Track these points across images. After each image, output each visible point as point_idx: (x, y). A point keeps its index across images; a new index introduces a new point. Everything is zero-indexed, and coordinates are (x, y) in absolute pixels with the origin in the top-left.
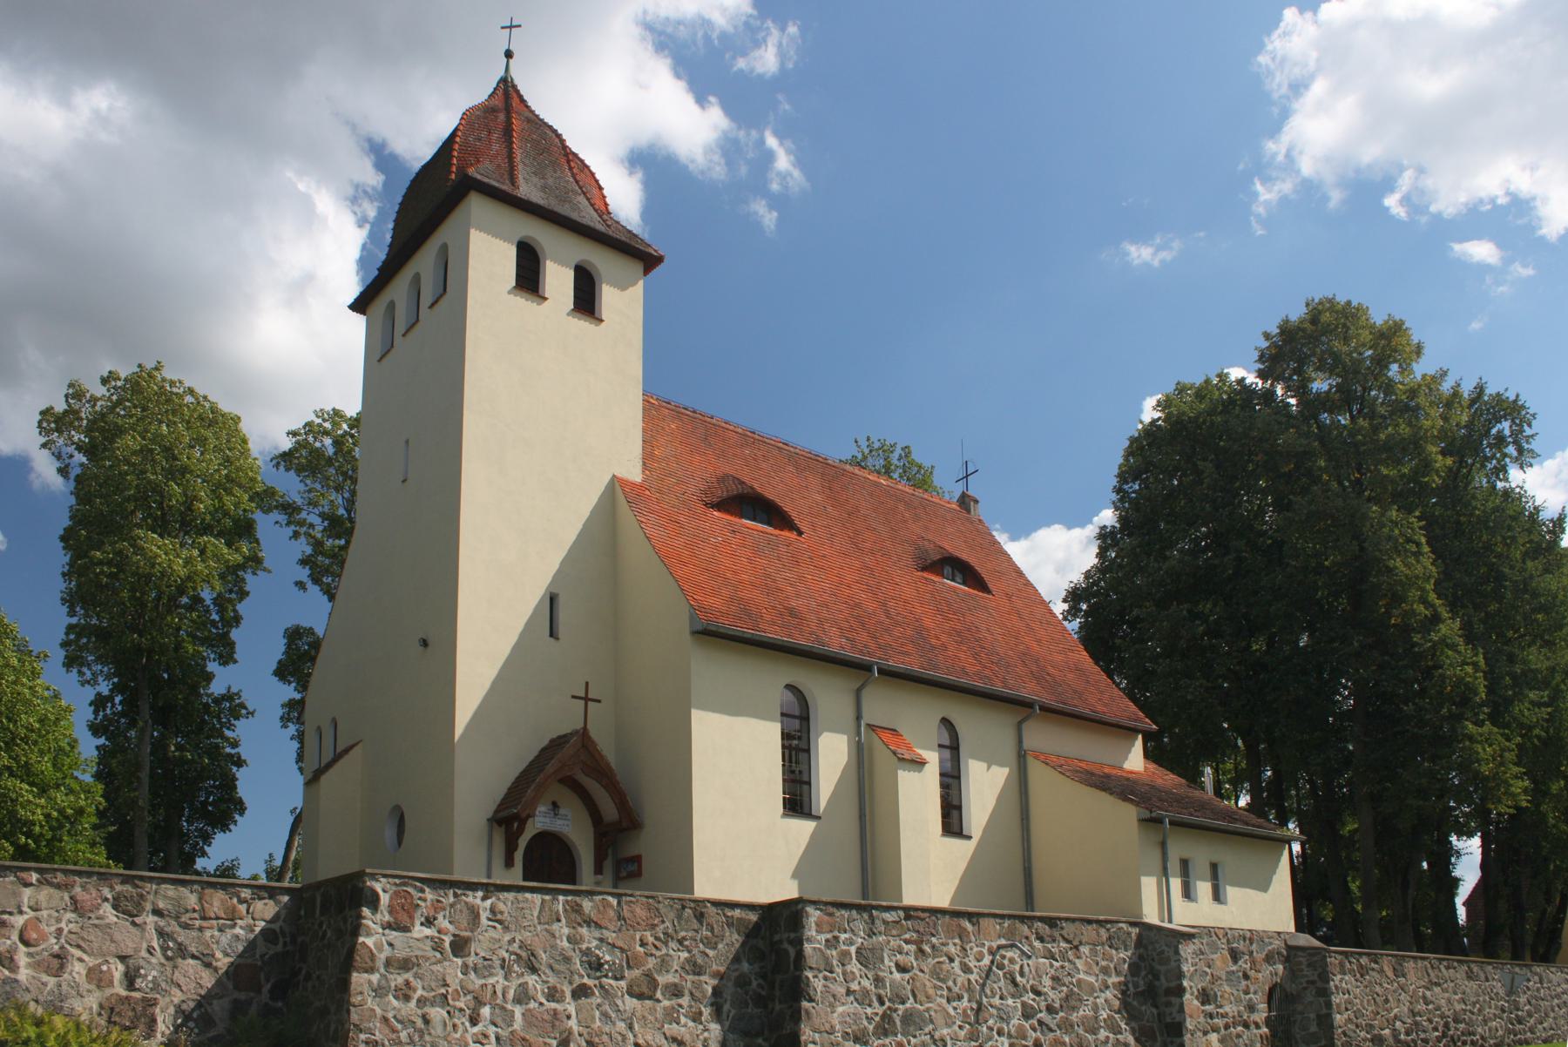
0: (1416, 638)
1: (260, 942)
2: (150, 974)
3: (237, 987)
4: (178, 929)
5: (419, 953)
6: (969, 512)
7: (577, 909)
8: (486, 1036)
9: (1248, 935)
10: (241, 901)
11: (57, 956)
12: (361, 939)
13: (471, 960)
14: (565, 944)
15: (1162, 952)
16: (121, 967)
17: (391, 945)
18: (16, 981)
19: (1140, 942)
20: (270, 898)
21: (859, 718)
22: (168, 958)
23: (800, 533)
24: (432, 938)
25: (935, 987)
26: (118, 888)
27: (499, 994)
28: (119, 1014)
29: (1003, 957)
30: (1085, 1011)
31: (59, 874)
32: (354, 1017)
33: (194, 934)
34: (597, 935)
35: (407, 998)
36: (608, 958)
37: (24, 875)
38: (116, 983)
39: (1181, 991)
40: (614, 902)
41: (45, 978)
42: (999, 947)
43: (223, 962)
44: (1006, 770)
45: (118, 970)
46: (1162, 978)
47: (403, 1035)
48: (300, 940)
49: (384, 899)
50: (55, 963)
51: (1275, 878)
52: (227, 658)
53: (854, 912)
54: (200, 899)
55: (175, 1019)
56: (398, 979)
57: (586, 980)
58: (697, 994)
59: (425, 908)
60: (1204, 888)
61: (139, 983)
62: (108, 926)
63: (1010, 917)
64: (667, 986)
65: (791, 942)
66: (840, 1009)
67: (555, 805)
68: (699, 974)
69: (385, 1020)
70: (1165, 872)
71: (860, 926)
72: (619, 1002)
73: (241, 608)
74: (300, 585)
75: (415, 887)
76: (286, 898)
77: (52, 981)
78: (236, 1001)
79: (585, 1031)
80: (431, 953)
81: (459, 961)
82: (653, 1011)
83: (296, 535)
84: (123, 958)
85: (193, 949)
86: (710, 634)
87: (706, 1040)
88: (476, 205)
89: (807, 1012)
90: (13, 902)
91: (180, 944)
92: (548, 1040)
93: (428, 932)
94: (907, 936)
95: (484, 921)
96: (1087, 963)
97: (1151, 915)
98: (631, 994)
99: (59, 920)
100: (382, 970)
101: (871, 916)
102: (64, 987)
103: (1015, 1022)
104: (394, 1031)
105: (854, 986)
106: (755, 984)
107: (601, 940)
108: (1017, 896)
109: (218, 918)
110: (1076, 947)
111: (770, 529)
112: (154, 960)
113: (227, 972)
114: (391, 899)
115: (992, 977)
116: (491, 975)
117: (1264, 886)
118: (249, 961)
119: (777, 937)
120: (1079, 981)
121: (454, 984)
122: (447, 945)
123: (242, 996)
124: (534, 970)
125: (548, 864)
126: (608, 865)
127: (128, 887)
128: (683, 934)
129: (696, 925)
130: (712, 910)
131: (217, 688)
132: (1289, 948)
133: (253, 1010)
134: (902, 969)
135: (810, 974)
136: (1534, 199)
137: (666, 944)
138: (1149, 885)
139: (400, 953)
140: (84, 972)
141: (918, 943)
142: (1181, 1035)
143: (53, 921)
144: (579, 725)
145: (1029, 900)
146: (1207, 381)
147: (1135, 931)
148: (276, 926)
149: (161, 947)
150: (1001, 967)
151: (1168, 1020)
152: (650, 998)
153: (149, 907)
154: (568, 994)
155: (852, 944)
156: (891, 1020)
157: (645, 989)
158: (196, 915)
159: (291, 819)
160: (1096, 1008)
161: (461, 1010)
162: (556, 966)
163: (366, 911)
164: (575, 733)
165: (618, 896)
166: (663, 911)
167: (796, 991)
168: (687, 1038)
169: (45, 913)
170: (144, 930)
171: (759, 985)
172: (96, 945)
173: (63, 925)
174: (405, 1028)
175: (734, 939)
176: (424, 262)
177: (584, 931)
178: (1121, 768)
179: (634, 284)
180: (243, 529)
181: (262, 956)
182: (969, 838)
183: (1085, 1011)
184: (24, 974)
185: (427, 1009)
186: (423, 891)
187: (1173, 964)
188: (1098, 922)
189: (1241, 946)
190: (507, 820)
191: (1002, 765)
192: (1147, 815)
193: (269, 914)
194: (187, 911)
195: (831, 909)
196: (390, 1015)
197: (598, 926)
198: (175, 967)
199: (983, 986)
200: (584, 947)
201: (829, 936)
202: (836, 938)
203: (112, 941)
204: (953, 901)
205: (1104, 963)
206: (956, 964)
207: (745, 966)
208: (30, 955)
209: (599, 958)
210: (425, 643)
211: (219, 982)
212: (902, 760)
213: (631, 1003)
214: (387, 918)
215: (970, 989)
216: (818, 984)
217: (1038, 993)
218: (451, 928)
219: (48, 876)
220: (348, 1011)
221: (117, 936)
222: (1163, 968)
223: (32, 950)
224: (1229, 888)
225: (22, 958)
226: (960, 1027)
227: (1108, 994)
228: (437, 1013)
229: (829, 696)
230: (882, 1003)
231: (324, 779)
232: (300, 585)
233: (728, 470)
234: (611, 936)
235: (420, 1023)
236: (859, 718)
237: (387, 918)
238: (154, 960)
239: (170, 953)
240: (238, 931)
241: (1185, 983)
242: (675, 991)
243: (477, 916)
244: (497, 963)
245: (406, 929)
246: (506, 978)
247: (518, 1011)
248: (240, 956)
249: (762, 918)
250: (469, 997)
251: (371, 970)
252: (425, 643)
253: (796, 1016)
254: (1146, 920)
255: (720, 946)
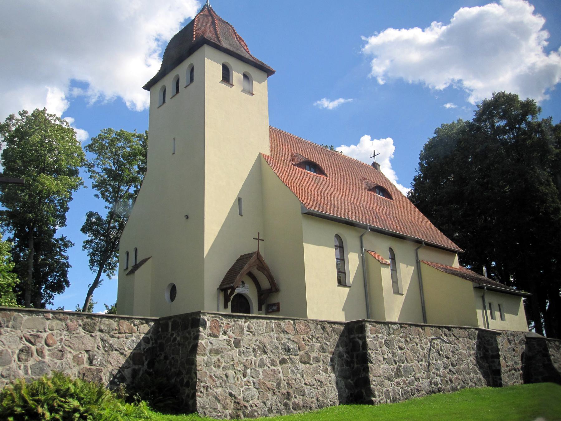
0: (552, 216)
1: (143, 342)
2: (99, 358)
3: (134, 363)
4: (109, 338)
5: (222, 347)
6: (377, 169)
7: (279, 326)
8: (249, 382)
9: (513, 333)
10: (135, 325)
11: (61, 351)
12: (200, 341)
13: (242, 349)
14: (276, 341)
15: (489, 341)
16: (87, 355)
17: (211, 343)
18: (44, 362)
19: (479, 337)
20: (147, 323)
21: (362, 247)
22: (106, 351)
23: (326, 176)
24: (227, 340)
25: (413, 356)
26: (85, 320)
27: (253, 363)
28: (87, 376)
29: (434, 343)
30: (464, 366)
31: (61, 314)
32: (198, 376)
33: (116, 340)
34: (287, 337)
35: (219, 367)
36: (292, 346)
37: (46, 315)
38: (85, 362)
39: (498, 356)
40: (292, 322)
41: (56, 361)
42: (433, 339)
43: (128, 352)
44: (413, 268)
45: (85, 356)
46: (490, 352)
47: (218, 383)
48: (159, 341)
49: (208, 323)
50: (60, 353)
51: (519, 310)
52: (63, 224)
53: (383, 325)
54: (118, 325)
55: (110, 378)
56: (215, 358)
57: (284, 356)
58: (325, 361)
59: (224, 328)
60: (497, 314)
61: (94, 362)
62: (81, 337)
63: (435, 327)
64: (314, 358)
65: (359, 338)
66: (382, 366)
67: (243, 283)
68: (325, 352)
69: (211, 376)
70: (484, 308)
71: (384, 331)
72: (297, 365)
73: (69, 204)
74: (97, 196)
75: (220, 318)
76: (152, 324)
77: (59, 362)
78: (134, 370)
79: (286, 378)
80: (227, 347)
81: (237, 349)
82: (310, 369)
83: (91, 177)
84: (87, 351)
85: (116, 347)
86: (309, 214)
87: (330, 381)
88: (207, 50)
89: (371, 368)
90: (42, 327)
91: (111, 345)
92: (273, 383)
93: (225, 337)
94: (401, 335)
95: (245, 332)
96: (462, 345)
97: (481, 326)
98: (301, 362)
99: (61, 335)
100: (208, 355)
101: (389, 327)
102: (64, 364)
103: (442, 370)
104: (214, 381)
105: (386, 357)
106: (345, 356)
107: (289, 339)
108: (421, 317)
109: (125, 333)
110: (458, 339)
111: (316, 174)
112: (100, 352)
113: (130, 356)
114: (211, 323)
115: (432, 352)
116: (250, 355)
117: (516, 314)
118: (139, 351)
119: (352, 336)
120: (461, 352)
121: (236, 360)
122: (232, 342)
123: (136, 367)
124: (265, 352)
125: (240, 306)
126: (263, 307)
127: (89, 320)
128: (318, 335)
129: (322, 332)
130: (327, 325)
131: (57, 236)
132: (526, 338)
133: (141, 373)
134: (401, 349)
135: (369, 351)
136: (377, 77)
137: (312, 340)
138: (479, 312)
139: (215, 347)
140: (72, 358)
141: (405, 337)
142: (500, 375)
143: (59, 335)
144: (256, 250)
145: (425, 320)
146: (453, 123)
147: (477, 332)
148: (149, 336)
149: (103, 346)
150: (434, 347)
151: (494, 368)
152: (308, 363)
153: (97, 328)
154: (278, 363)
155: (383, 338)
156: (400, 371)
157: (306, 360)
158: (116, 332)
159: (88, 289)
160: (468, 364)
161: (240, 371)
162: (273, 351)
163: (201, 329)
164: (255, 253)
165: (294, 320)
166: (310, 325)
167: (364, 359)
168: (323, 380)
169: (55, 332)
170: (95, 339)
171: (347, 357)
172: (76, 346)
173: (63, 337)
174: (218, 380)
175: (336, 337)
176: (182, 70)
177: (282, 335)
178: (452, 267)
179: (264, 81)
180: (73, 173)
181: (144, 349)
182: (402, 294)
183: (464, 366)
184: (47, 359)
185: (227, 371)
186: (222, 320)
187: (494, 345)
188: (464, 328)
189: (511, 338)
190: (226, 289)
191: (412, 266)
192: (477, 285)
193: (146, 331)
194: (113, 330)
195: (375, 324)
196: (212, 374)
197: (287, 333)
198: (109, 355)
199: (429, 355)
200: (283, 342)
201: (375, 335)
202: (377, 336)
203: (83, 344)
204: (399, 320)
205: (468, 345)
206: (419, 346)
207: (341, 349)
208: (49, 350)
209: (289, 347)
210: (187, 217)
211: (127, 361)
212: (382, 263)
213: (301, 366)
214: (209, 332)
215: (425, 357)
216: (373, 355)
217: (448, 358)
218: (233, 335)
219: (57, 315)
220: (196, 374)
221: (85, 341)
222: (489, 347)
223: (50, 348)
224: (505, 314)
225: (46, 352)
226: (424, 373)
227: (471, 358)
228: (231, 373)
229: (350, 238)
230: (396, 364)
231: (137, 272)
232: (97, 196)
233: (296, 151)
234: (292, 337)
235: (224, 377)
236: (362, 247)
237: (209, 332)
238: (100, 352)
239: (106, 349)
240: (134, 338)
241: (500, 353)
242: (317, 360)
243: (243, 330)
244: (252, 350)
245: (216, 336)
246: (255, 356)
247: (261, 370)
248: (135, 349)
249: (345, 328)
250: (242, 365)
251: (204, 355)
252: (187, 217)
253: (367, 370)
254: (480, 328)
255: (331, 340)
